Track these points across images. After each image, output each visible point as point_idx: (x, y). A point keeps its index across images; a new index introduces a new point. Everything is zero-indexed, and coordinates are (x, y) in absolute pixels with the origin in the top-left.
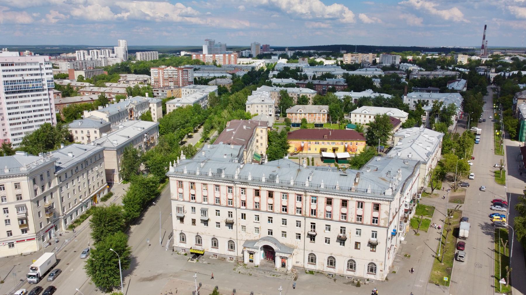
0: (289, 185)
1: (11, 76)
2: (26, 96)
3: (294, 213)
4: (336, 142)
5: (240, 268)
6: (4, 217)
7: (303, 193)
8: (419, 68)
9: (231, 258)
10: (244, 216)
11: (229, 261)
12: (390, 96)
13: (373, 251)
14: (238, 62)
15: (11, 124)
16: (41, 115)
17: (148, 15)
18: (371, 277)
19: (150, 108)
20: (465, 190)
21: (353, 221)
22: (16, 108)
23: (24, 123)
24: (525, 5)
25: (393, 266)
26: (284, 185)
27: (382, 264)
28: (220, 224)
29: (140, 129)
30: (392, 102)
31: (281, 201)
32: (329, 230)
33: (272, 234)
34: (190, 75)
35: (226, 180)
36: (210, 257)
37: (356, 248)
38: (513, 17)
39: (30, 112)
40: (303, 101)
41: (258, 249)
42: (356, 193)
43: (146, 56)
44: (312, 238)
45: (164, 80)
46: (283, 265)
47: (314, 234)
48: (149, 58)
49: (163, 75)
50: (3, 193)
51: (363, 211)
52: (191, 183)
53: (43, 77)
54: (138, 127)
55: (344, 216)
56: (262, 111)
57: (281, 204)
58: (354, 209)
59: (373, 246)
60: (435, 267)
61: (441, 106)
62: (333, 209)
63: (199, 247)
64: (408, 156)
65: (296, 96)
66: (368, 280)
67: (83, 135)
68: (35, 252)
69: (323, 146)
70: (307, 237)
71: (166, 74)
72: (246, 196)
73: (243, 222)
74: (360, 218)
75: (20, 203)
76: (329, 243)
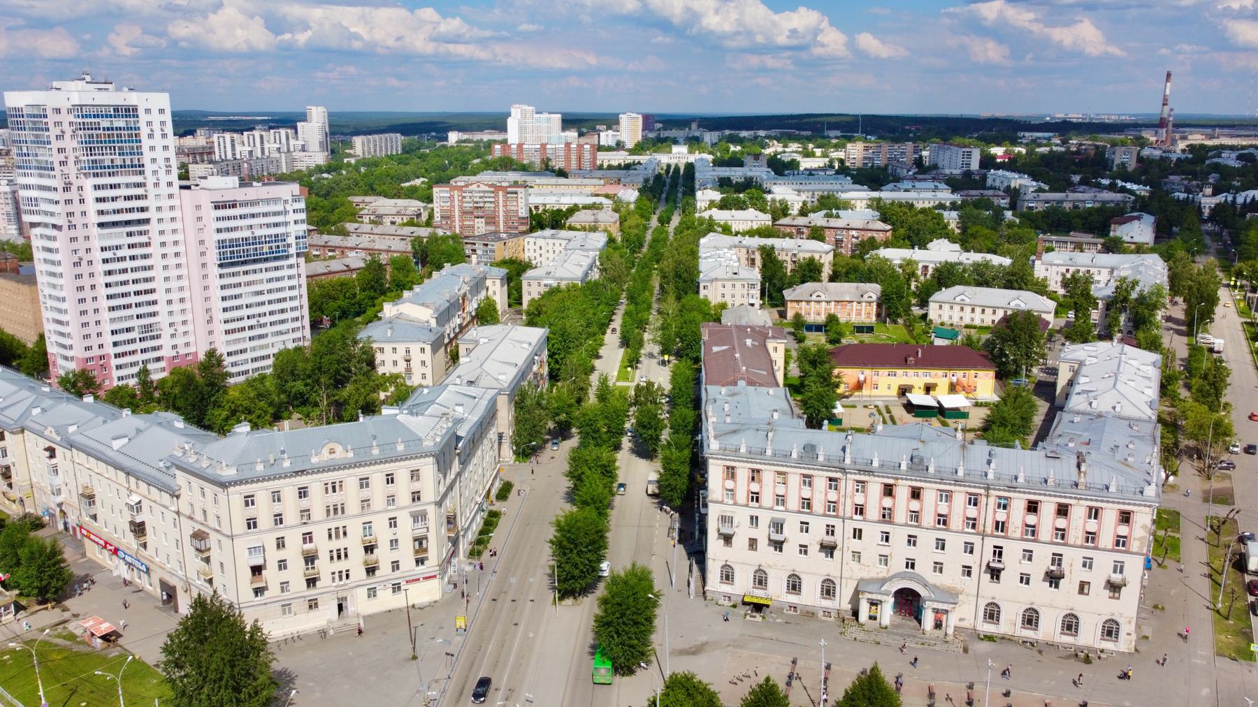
2: (255, 271)
4: (933, 372)
8: (1034, 183)
9: (827, 613)
12: (1007, 261)
13: (1113, 597)
14: (599, 163)
15: (227, 332)
16: (282, 311)
17: (356, 36)
21: (1079, 542)
23: (251, 328)
24: (1257, 16)
26: (945, 475)
28: (809, 549)
31: (937, 505)
32: (1030, 559)
33: (913, 566)
34: (521, 203)
35: (826, 466)
38: (1226, 45)
39: (263, 303)
40: (811, 271)
44: (995, 573)
45: (464, 213)
49: (461, 201)
52: (753, 471)
54: (521, 342)
56: (733, 296)
61: (1133, 288)
64: (1114, 408)
65: (788, 259)
66: (1102, 651)
73: (856, 544)
74: (1091, 537)
75: (418, 507)
76: (1027, 583)
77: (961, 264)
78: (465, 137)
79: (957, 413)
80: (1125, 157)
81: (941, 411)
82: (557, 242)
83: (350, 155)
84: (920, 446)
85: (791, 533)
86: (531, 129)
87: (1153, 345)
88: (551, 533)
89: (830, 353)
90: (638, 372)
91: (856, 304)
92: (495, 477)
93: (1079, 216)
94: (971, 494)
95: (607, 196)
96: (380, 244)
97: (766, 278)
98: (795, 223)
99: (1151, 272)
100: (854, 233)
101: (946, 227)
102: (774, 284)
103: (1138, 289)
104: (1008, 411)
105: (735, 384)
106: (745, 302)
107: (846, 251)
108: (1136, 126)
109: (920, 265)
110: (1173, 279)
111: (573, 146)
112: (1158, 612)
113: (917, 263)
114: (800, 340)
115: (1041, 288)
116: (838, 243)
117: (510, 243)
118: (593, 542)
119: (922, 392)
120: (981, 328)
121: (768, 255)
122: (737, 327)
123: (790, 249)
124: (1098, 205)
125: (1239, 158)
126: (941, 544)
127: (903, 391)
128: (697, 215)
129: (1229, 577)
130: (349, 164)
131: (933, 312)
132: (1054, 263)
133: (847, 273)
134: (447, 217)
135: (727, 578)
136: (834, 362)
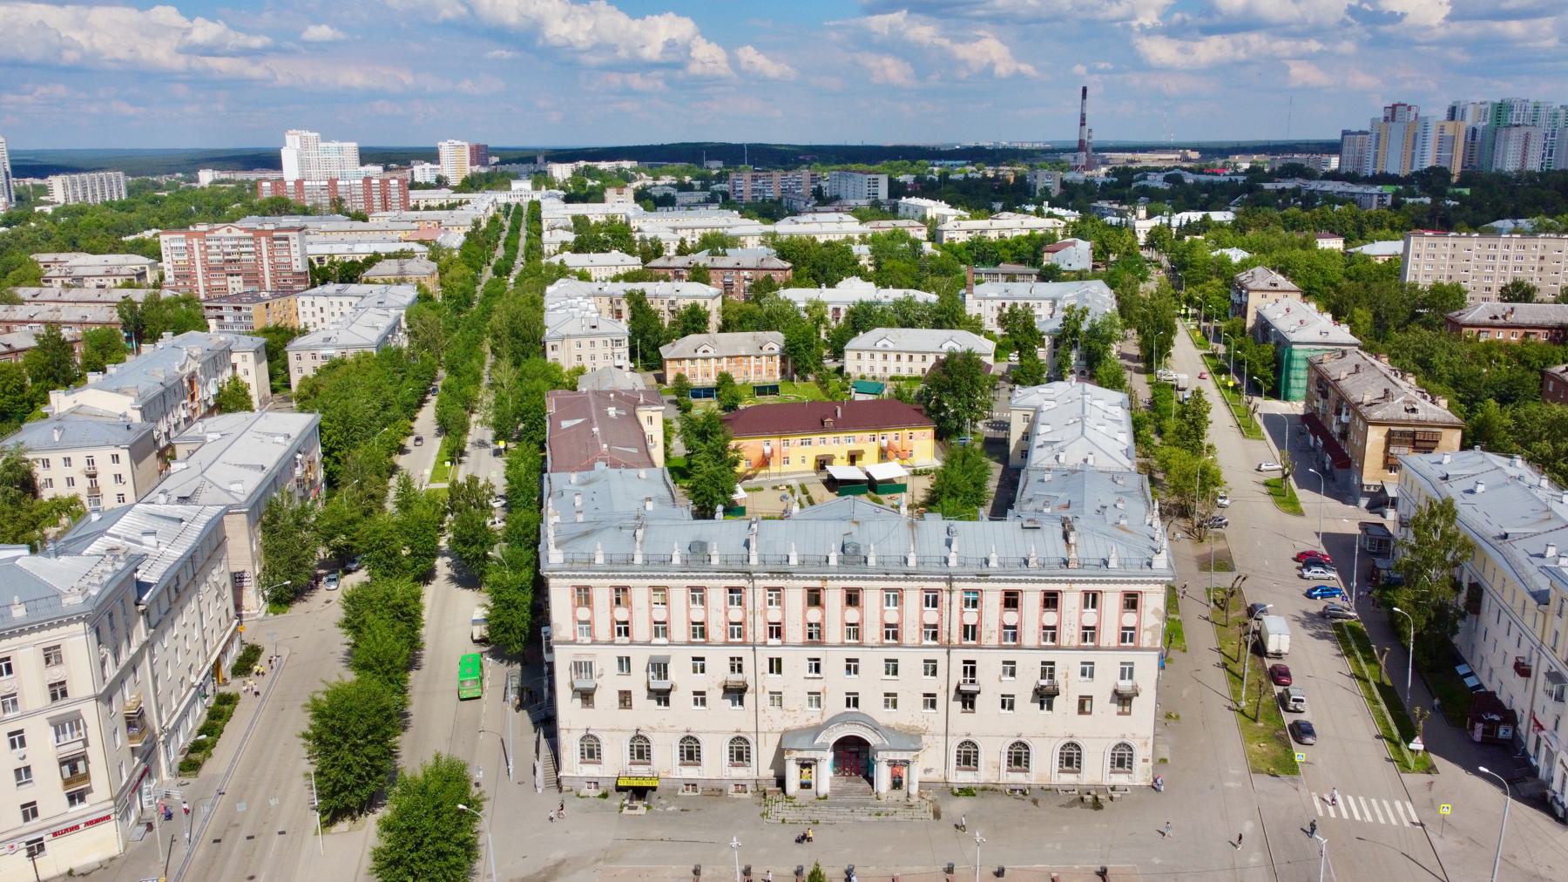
4: (858, 435)
6: (13, 759)
7: (943, 585)
8: (953, 211)
9: (741, 787)
11: (737, 795)
12: (933, 297)
14: (412, 204)
18: (1121, 779)
26: (890, 568)
28: (707, 697)
30: (942, 312)
31: (883, 612)
32: (1013, 674)
33: (856, 704)
34: (296, 253)
35: (722, 572)
38: (1140, 65)
40: (694, 321)
42: (1081, 572)
43: (85, 189)
44: (968, 700)
45: (210, 269)
48: (94, 196)
49: (205, 253)
50: (6, 684)
52: (617, 590)
54: (273, 435)
56: (593, 358)
58: (1076, 612)
59: (1123, 699)
60: (1248, 738)
61: (1083, 318)
64: (1086, 461)
65: (664, 308)
66: (1113, 789)
67: (69, 472)
68: (112, 859)
69: (823, 450)
72: (784, 610)
73: (774, 682)
74: (1089, 633)
75: (63, 709)
76: (1011, 707)
77: (878, 303)
78: (224, 176)
79: (891, 486)
80: (1047, 180)
81: (871, 486)
82: (345, 300)
83: (47, 203)
84: (854, 528)
85: (681, 676)
86: (310, 159)
87: (1115, 383)
88: (304, 722)
89: (723, 421)
90: (462, 467)
91: (754, 359)
92: (231, 640)
93: (1007, 245)
94: (927, 591)
95: (421, 242)
96: (68, 313)
97: (635, 334)
98: (671, 264)
99: (1100, 300)
100: (746, 273)
101: (856, 262)
102: (646, 342)
103: (1088, 319)
104: (960, 480)
105: (591, 467)
106: (610, 363)
107: (737, 298)
108: (1052, 151)
109: (830, 308)
110: (1124, 308)
112: (1172, 722)
113: (825, 304)
114: (685, 409)
115: (975, 327)
116: (728, 287)
117: (276, 305)
118: (373, 729)
119: (846, 462)
120: (910, 379)
121: (638, 303)
122: (595, 392)
123: (668, 296)
124: (1026, 233)
125: (1166, 179)
126: (892, 667)
127: (822, 463)
128: (544, 261)
129: (1248, 663)
130: (43, 214)
131: (851, 363)
132: (986, 299)
133: (741, 322)
134: (185, 275)
135: (591, 754)
136: (729, 430)
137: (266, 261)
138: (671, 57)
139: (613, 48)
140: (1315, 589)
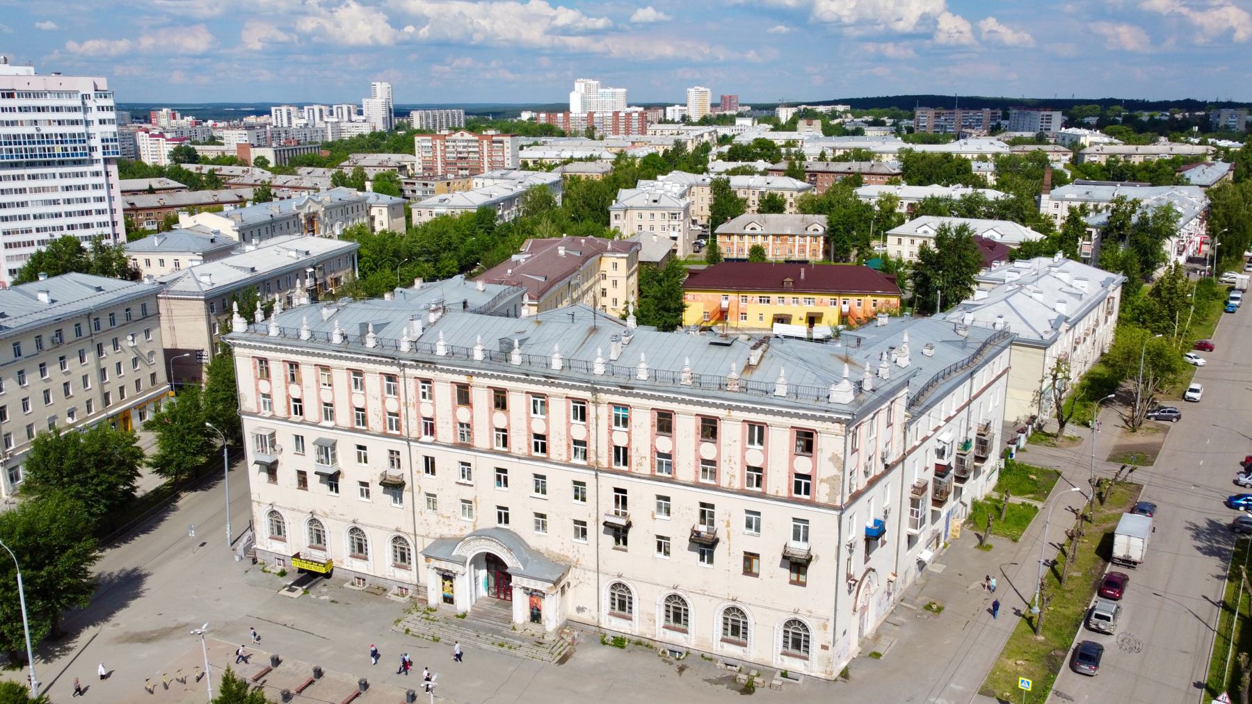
0: (548, 371)
1: (7, 124)
2: (45, 176)
3: (564, 458)
5: (414, 622)
7: (587, 395)
9: (403, 590)
10: (430, 465)
11: (394, 598)
18: (794, 665)
19: (373, 219)
20: (1166, 430)
21: (737, 485)
22: (23, 204)
25: (877, 636)
26: (534, 368)
27: (825, 627)
29: (293, 254)
31: (529, 420)
36: (347, 585)
37: (748, 570)
39: (58, 215)
41: (464, 564)
44: (620, 533)
45: (447, 164)
46: (536, 617)
47: (622, 522)
51: (765, 453)
53: (91, 130)
54: (289, 250)
55: (709, 466)
57: (529, 428)
58: (738, 447)
59: (798, 566)
61: (1133, 211)
62: (674, 445)
63: (318, 555)
69: (782, 309)
70: (605, 532)
71: (451, 149)
72: (434, 405)
73: (427, 482)
74: (757, 474)
111: (622, 114)
137: (486, 159)
138: (923, 29)
139: (873, 22)
140: (1239, 497)
